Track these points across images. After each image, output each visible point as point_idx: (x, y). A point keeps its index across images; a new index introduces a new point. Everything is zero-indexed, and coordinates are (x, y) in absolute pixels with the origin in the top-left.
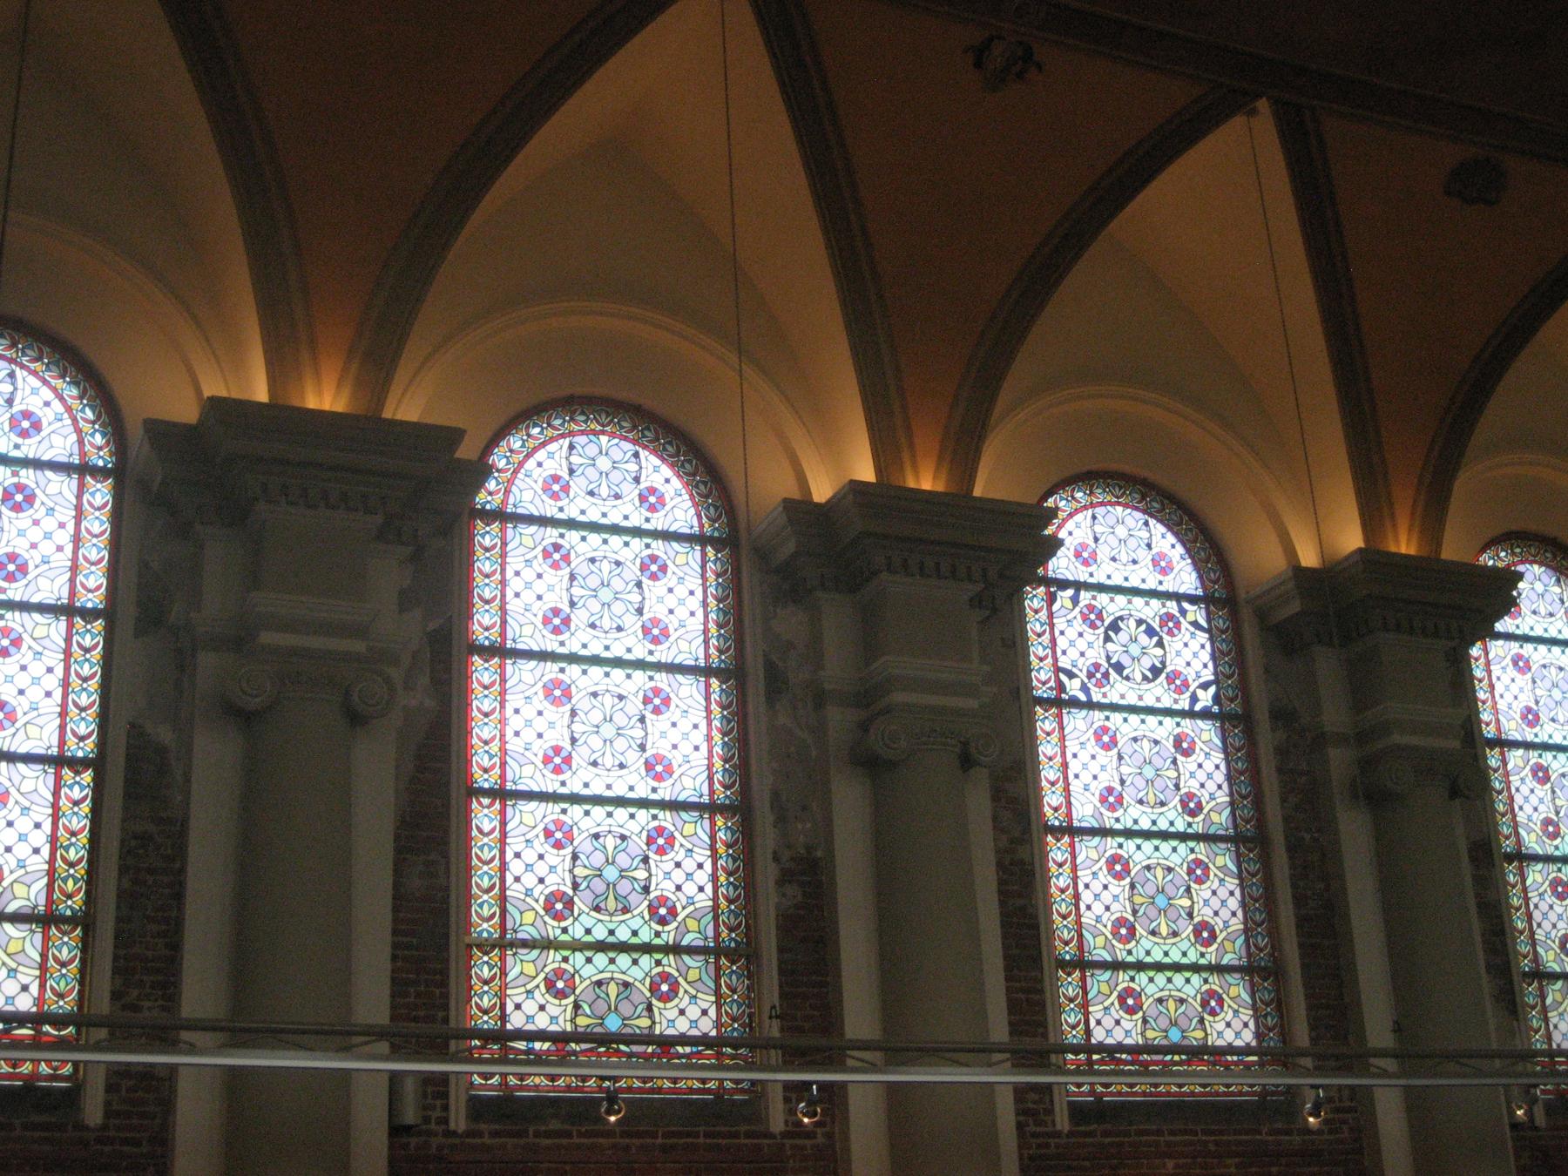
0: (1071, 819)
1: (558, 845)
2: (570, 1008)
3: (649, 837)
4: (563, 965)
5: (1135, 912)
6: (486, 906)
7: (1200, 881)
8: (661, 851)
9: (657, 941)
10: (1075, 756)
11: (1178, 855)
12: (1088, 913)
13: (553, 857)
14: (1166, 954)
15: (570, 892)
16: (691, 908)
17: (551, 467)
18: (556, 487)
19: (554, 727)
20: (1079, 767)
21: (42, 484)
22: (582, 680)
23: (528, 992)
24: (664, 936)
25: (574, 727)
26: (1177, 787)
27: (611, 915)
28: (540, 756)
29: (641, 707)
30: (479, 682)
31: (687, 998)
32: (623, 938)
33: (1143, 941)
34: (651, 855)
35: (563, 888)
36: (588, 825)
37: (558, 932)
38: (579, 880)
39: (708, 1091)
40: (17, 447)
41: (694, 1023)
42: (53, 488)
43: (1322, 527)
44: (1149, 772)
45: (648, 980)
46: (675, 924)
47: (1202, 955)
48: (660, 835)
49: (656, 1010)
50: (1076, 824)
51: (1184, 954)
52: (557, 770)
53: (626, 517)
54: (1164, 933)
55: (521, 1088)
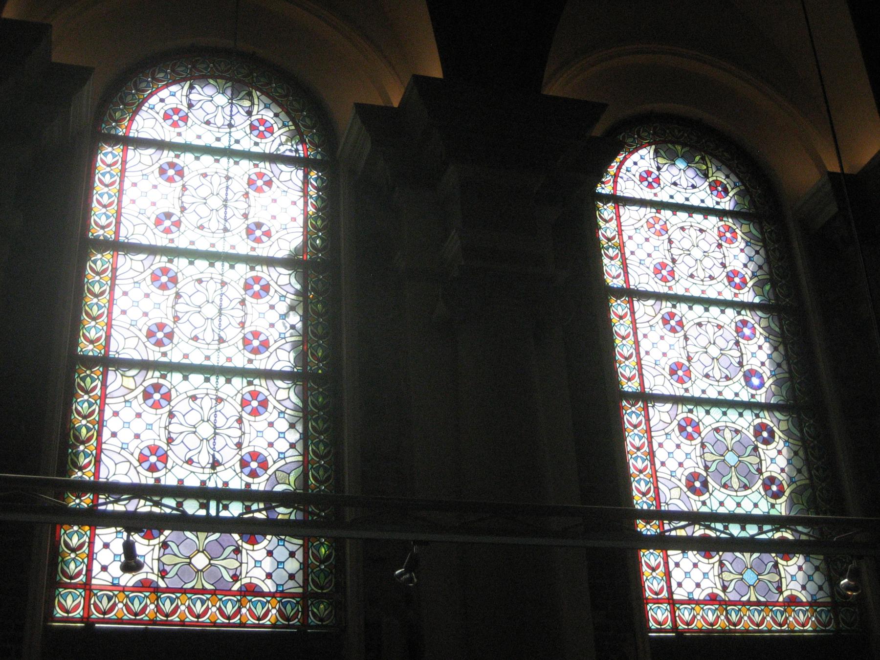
0: (644, 388)
1: (690, 437)
2: (717, 564)
3: (243, 400)
5: (707, 468)
6: (642, 483)
7: (766, 442)
10: (645, 336)
11: (747, 421)
12: (663, 469)
13: (686, 446)
14: (739, 505)
16: (282, 462)
17: (172, 103)
18: (176, 117)
19: (158, 307)
20: (648, 348)
21: (277, 174)
22: (691, 314)
25: (177, 307)
26: (741, 364)
28: (145, 331)
29: (243, 292)
30: (615, 314)
33: (716, 493)
34: (759, 445)
35: (698, 470)
37: (700, 504)
38: (709, 464)
39: (293, 626)
40: (256, 144)
42: (285, 176)
43: (842, 155)
44: (714, 351)
47: (773, 506)
50: (112, 354)
51: (756, 505)
52: (159, 343)
53: (199, 137)
54: (736, 486)
55: (689, 631)
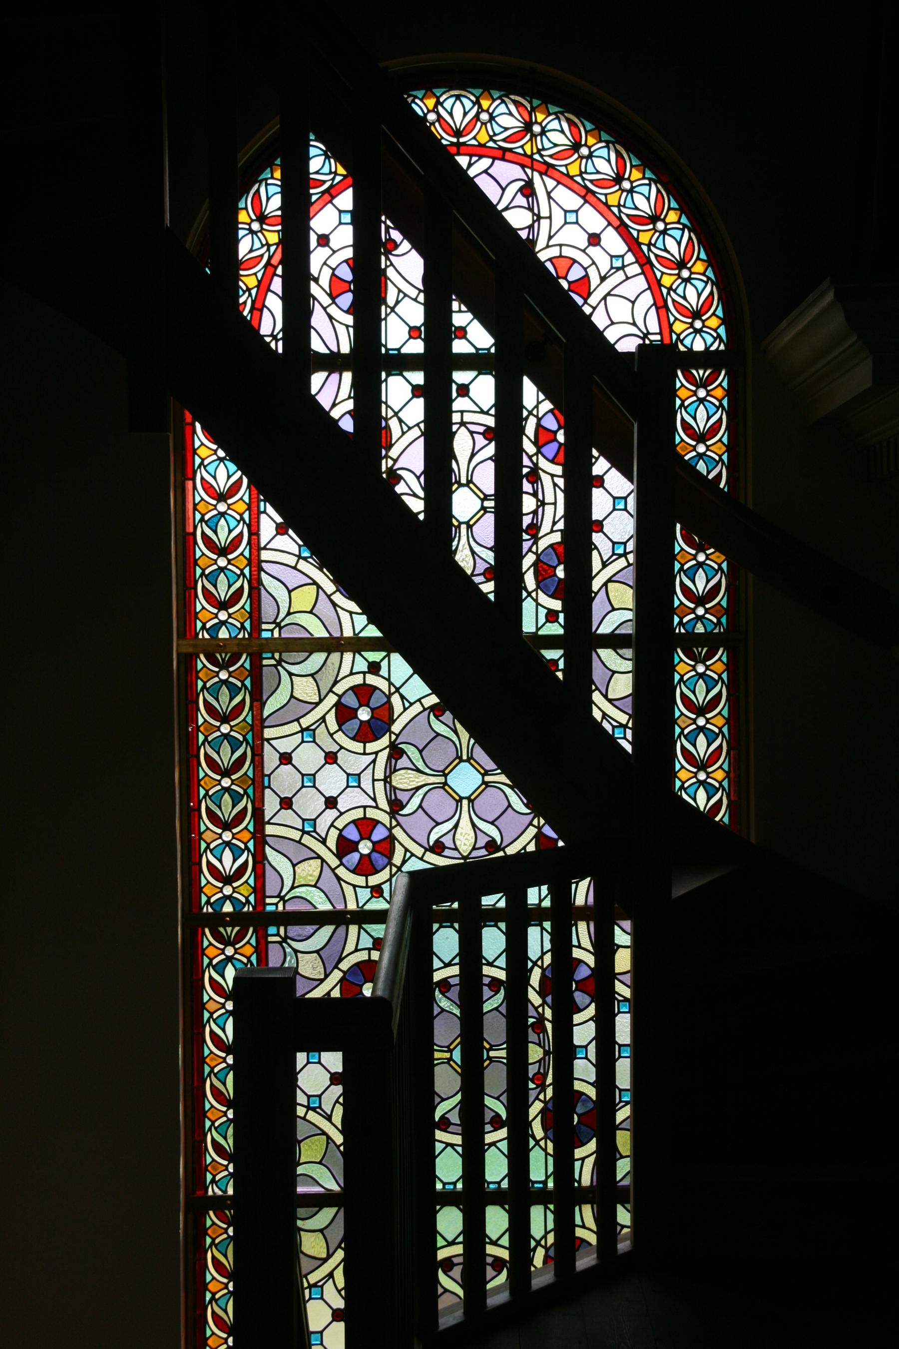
4: (371, 680)
23: (302, 730)
38: (403, 797)
49: (383, 803)
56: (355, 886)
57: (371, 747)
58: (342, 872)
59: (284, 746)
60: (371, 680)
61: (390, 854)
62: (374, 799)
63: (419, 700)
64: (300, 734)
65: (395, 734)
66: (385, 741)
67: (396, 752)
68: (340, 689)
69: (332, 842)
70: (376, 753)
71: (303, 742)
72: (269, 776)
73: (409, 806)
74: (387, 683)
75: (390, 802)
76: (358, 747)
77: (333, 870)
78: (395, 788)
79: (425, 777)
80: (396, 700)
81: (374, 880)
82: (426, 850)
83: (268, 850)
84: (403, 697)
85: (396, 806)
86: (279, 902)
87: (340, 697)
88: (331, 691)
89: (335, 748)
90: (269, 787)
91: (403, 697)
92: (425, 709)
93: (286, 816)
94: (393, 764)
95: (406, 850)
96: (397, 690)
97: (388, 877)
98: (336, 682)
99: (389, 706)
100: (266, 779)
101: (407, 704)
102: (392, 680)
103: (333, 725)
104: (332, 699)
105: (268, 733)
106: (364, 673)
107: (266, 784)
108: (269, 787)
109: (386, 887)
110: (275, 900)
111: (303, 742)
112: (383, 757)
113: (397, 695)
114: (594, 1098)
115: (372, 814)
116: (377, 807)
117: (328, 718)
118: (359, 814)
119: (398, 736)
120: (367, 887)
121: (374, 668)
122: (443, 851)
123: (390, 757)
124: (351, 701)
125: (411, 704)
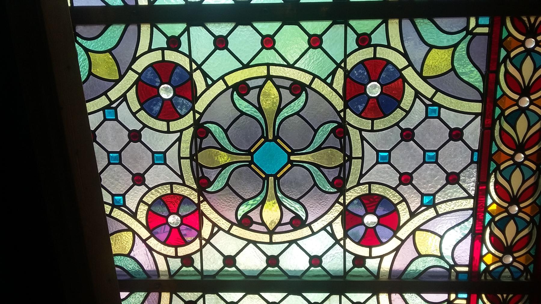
4: (363, 251)
8: (171, 202)
9: (175, 29)
15: (351, 118)
23: (434, 205)
24: (160, 41)
27: (269, 77)
31: (131, 204)
32: (244, 31)
36: (318, 244)
38: (334, 141)
41: (116, 158)
45: (206, 231)
46: (139, 66)
48: (175, 231)
49: (190, 180)
56: (389, 46)
57: (175, 125)
58: (401, 62)
59: (454, 191)
60: (171, 56)
61: (199, 229)
62: (363, 139)
63: (222, 78)
64: (437, 202)
65: (198, 113)
66: (188, 120)
67: (200, 130)
68: (395, 243)
69: (142, 215)
70: (181, 131)
71: (105, 119)
72: (472, 162)
73: (216, 183)
74: (347, 248)
75: (197, 180)
76: (161, 125)
77: (410, 64)
78: (202, 166)
79: (312, 160)
80: (339, 232)
81: (367, 53)
82: (309, 86)
83: (480, 85)
84: (205, 75)
85: (341, 131)
86: (474, 28)
87: (395, 235)
88: (403, 242)
89: (139, 126)
90: (473, 151)
91: (205, 75)
92: (228, 88)
93: (456, 121)
94: (198, 143)
95: (330, 85)
96: (199, 67)
97: (348, 60)
98: (397, 249)
99: (346, 227)
100: (475, 159)
101: (210, 82)
102: (194, 56)
103: (402, 209)
104: (403, 233)
105: (470, 203)
106: (163, 49)
107: (476, 154)
108: (473, 151)
109: (352, 45)
110: (479, 30)
111: (105, 119)
112: (188, 135)
113: (339, 238)
114: (203, 3)
115: (179, 190)
116: (360, 130)
117: (408, 216)
118: (166, 190)
119: (202, 114)
120: (375, 46)
121: (174, 43)
122: (291, 85)
123: (195, 136)
124: (383, 232)
125: (214, 82)
